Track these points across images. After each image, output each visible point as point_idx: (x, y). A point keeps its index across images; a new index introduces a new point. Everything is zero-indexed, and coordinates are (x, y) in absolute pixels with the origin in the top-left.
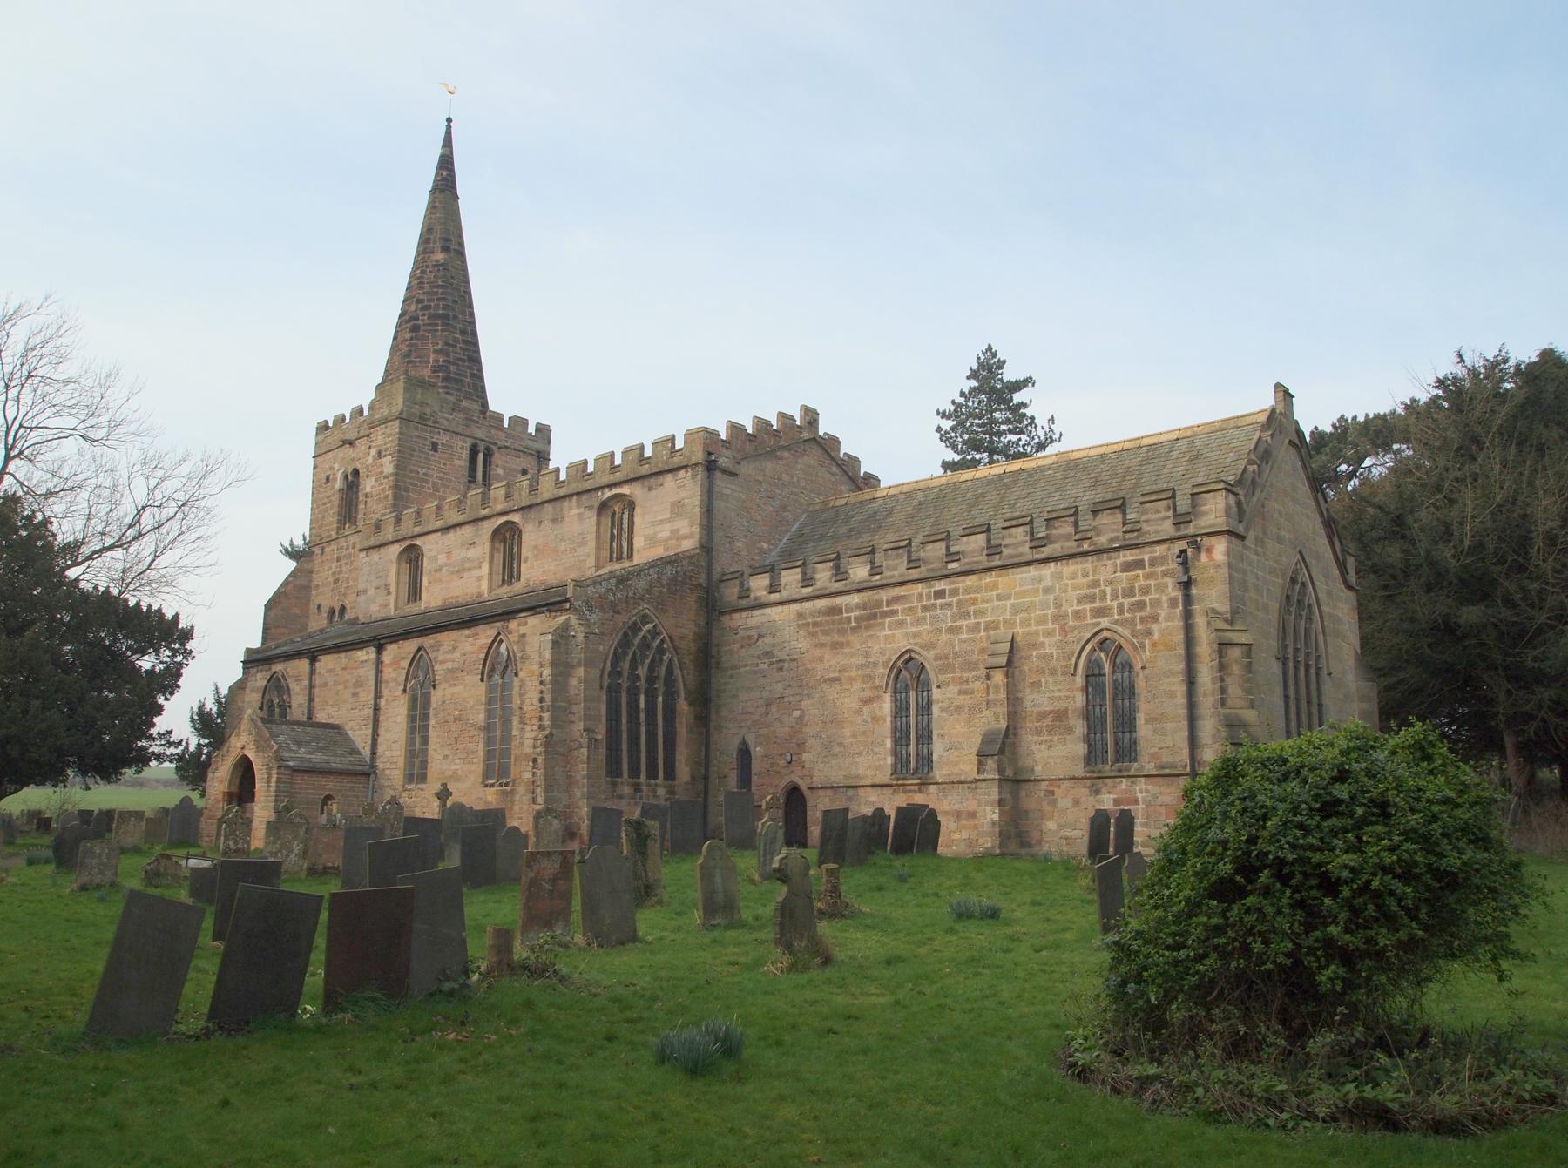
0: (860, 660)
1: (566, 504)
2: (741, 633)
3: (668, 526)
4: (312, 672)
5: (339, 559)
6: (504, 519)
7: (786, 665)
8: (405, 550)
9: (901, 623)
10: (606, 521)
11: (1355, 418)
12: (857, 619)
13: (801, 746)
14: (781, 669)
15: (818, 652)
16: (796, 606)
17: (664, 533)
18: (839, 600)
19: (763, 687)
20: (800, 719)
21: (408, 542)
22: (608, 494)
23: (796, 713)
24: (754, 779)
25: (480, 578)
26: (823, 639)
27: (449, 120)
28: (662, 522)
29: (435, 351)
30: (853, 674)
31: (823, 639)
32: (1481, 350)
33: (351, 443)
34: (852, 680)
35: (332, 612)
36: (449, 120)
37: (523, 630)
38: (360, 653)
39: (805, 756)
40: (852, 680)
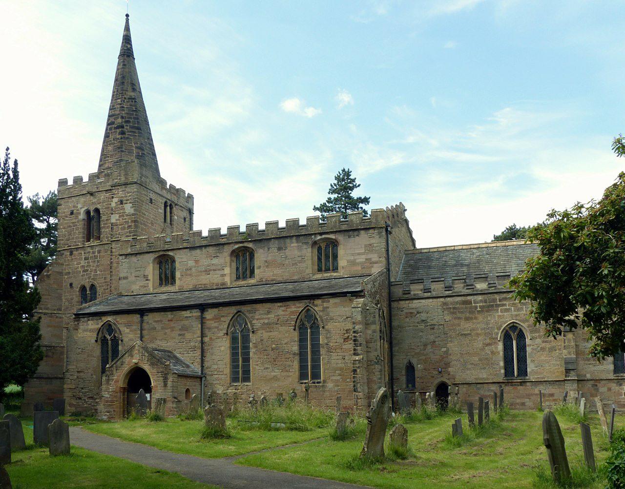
0: (483, 326)
1: (288, 241)
2: (406, 311)
3: (363, 256)
4: (142, 322)
5: (85, 259)
6: (241, 245)
7: (436, 327)
8: (159, 257)
9: (507, 310)
10: (316, 251)
11: (529, 227)
12: (480, 307)
13: (448, 365)
14: (433, 329)
15: (456, 322)
16: (442, 300)
17: (361, 259)
18: (469, 298)
19: (421, 337)
20: (446, 352)
21: (161, 253)
22: (319, 237)
23: (444, 349)
24: (417, 380)
25: (223, 275)
26: (459, 315)
27: (127, 16)
28: (359, 254)
29: (137, 148)
30: (480, 331)
31: (459, 315)
32: (565, 205)
33: (92, 194)
34: (478, 335)
35: (83, 288)
36: (127, 16)
37: (325, 305)
38: (184, 312)
39: (450, 369)
40: (478, 335)
